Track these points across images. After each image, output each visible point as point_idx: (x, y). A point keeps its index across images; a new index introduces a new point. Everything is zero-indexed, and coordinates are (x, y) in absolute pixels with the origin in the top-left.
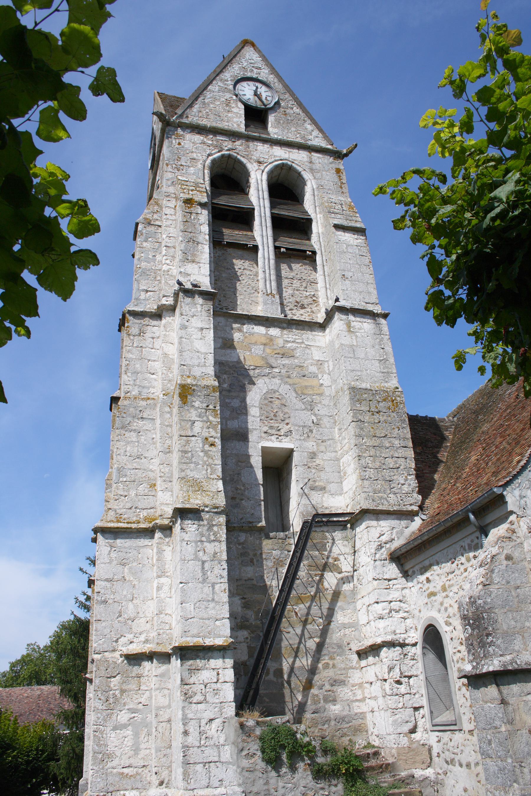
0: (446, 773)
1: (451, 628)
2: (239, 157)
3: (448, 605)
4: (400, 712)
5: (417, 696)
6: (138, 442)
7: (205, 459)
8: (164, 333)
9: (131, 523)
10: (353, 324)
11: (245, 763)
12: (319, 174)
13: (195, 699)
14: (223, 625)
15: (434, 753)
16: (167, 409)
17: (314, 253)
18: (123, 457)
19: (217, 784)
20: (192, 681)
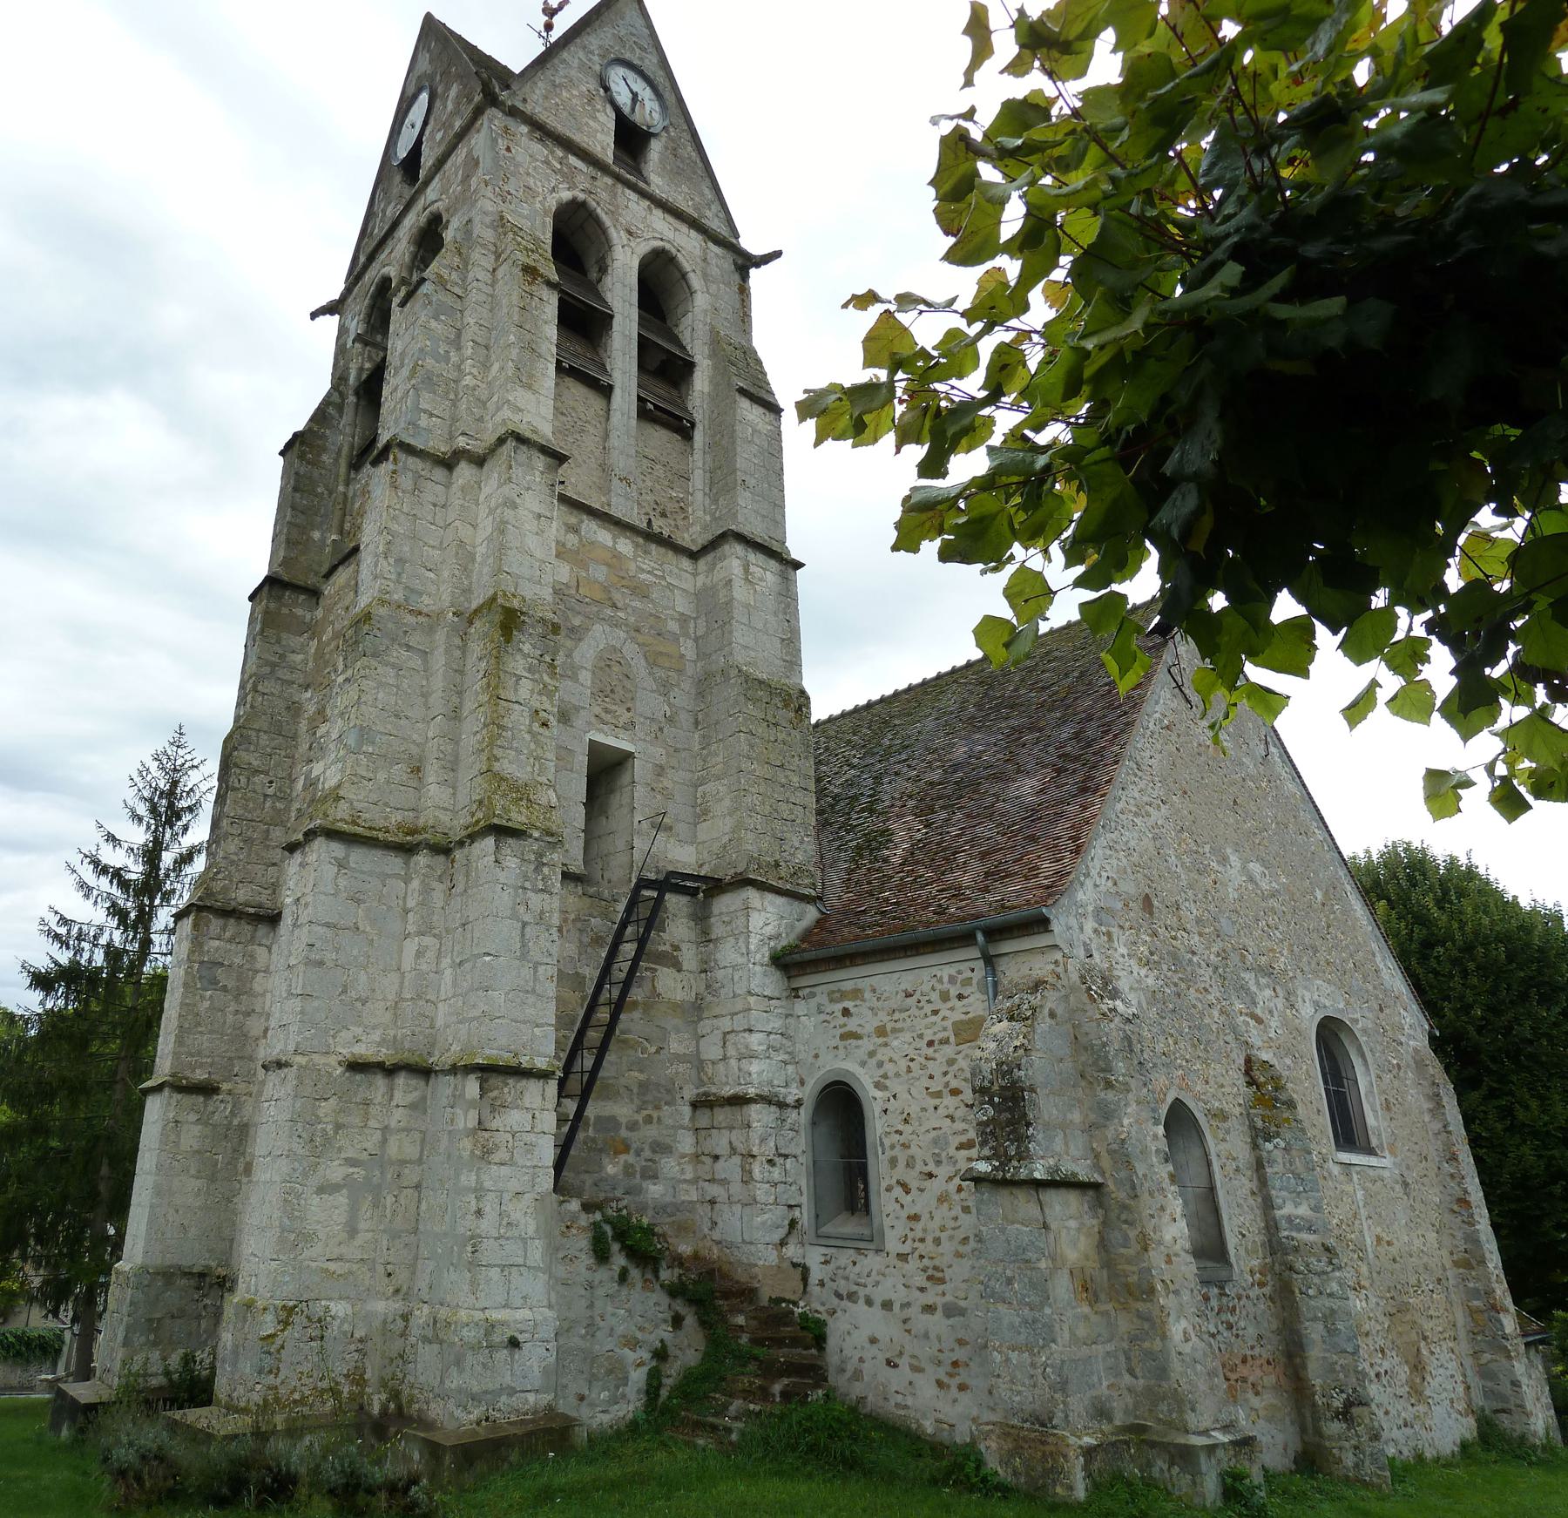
0: (833, 1313)
1: (887, 1094)
2: (599, 210)
3: (886, 1058)
4: (770, 1210)
5: (793, 1188)
6: (397, 687)
7: (533, 746)
8: (461, 502)
9: (374, 829)
10: (752, 568)
11: (561, 1271)
12: (714, 287)
13: (496, 1158)
14: (546, 1036)
15: (814, 1277)
16: (458, 641)
17: (693, 425)
18: (371, 709)
19: (518, 1302)
20: (494, 1125)
